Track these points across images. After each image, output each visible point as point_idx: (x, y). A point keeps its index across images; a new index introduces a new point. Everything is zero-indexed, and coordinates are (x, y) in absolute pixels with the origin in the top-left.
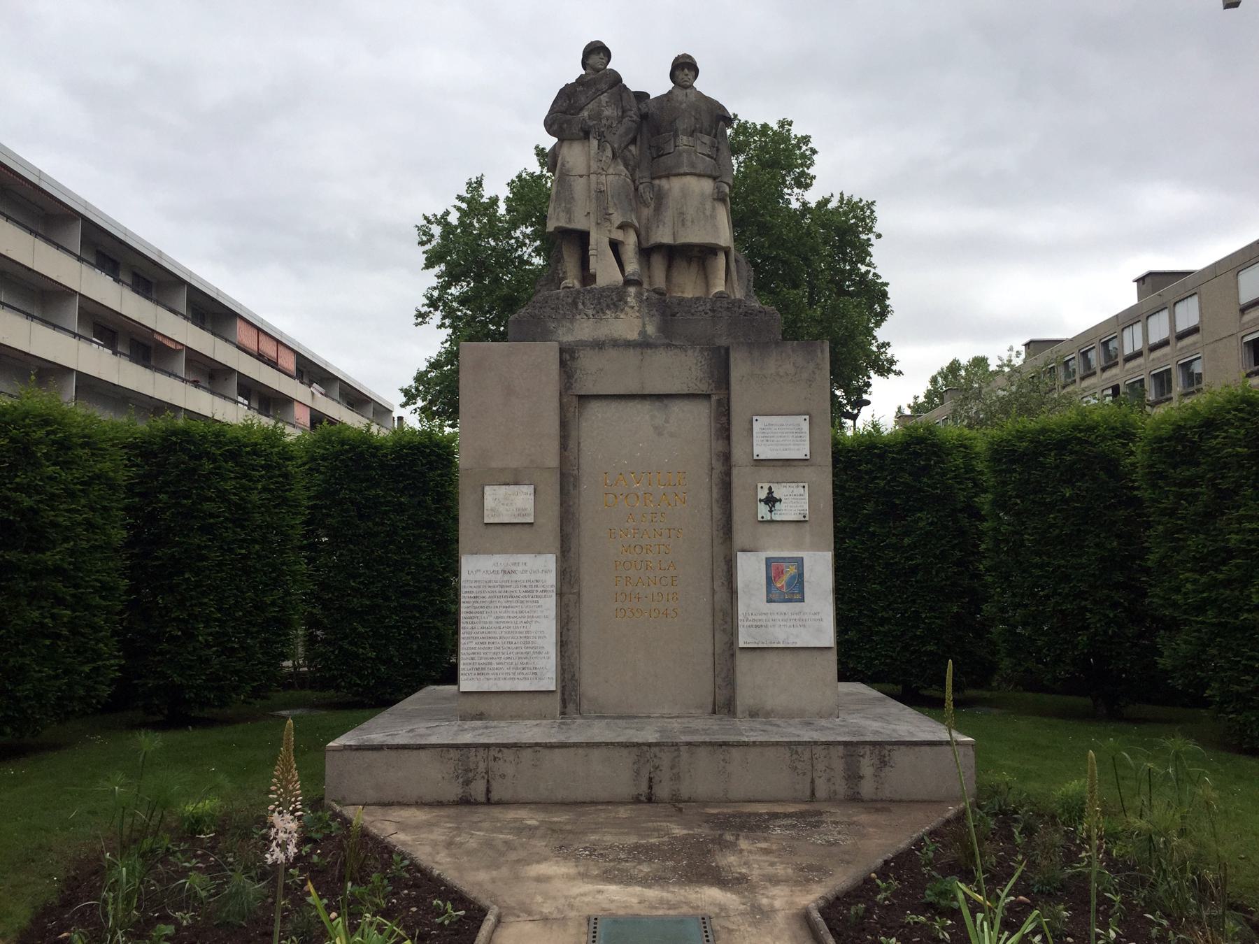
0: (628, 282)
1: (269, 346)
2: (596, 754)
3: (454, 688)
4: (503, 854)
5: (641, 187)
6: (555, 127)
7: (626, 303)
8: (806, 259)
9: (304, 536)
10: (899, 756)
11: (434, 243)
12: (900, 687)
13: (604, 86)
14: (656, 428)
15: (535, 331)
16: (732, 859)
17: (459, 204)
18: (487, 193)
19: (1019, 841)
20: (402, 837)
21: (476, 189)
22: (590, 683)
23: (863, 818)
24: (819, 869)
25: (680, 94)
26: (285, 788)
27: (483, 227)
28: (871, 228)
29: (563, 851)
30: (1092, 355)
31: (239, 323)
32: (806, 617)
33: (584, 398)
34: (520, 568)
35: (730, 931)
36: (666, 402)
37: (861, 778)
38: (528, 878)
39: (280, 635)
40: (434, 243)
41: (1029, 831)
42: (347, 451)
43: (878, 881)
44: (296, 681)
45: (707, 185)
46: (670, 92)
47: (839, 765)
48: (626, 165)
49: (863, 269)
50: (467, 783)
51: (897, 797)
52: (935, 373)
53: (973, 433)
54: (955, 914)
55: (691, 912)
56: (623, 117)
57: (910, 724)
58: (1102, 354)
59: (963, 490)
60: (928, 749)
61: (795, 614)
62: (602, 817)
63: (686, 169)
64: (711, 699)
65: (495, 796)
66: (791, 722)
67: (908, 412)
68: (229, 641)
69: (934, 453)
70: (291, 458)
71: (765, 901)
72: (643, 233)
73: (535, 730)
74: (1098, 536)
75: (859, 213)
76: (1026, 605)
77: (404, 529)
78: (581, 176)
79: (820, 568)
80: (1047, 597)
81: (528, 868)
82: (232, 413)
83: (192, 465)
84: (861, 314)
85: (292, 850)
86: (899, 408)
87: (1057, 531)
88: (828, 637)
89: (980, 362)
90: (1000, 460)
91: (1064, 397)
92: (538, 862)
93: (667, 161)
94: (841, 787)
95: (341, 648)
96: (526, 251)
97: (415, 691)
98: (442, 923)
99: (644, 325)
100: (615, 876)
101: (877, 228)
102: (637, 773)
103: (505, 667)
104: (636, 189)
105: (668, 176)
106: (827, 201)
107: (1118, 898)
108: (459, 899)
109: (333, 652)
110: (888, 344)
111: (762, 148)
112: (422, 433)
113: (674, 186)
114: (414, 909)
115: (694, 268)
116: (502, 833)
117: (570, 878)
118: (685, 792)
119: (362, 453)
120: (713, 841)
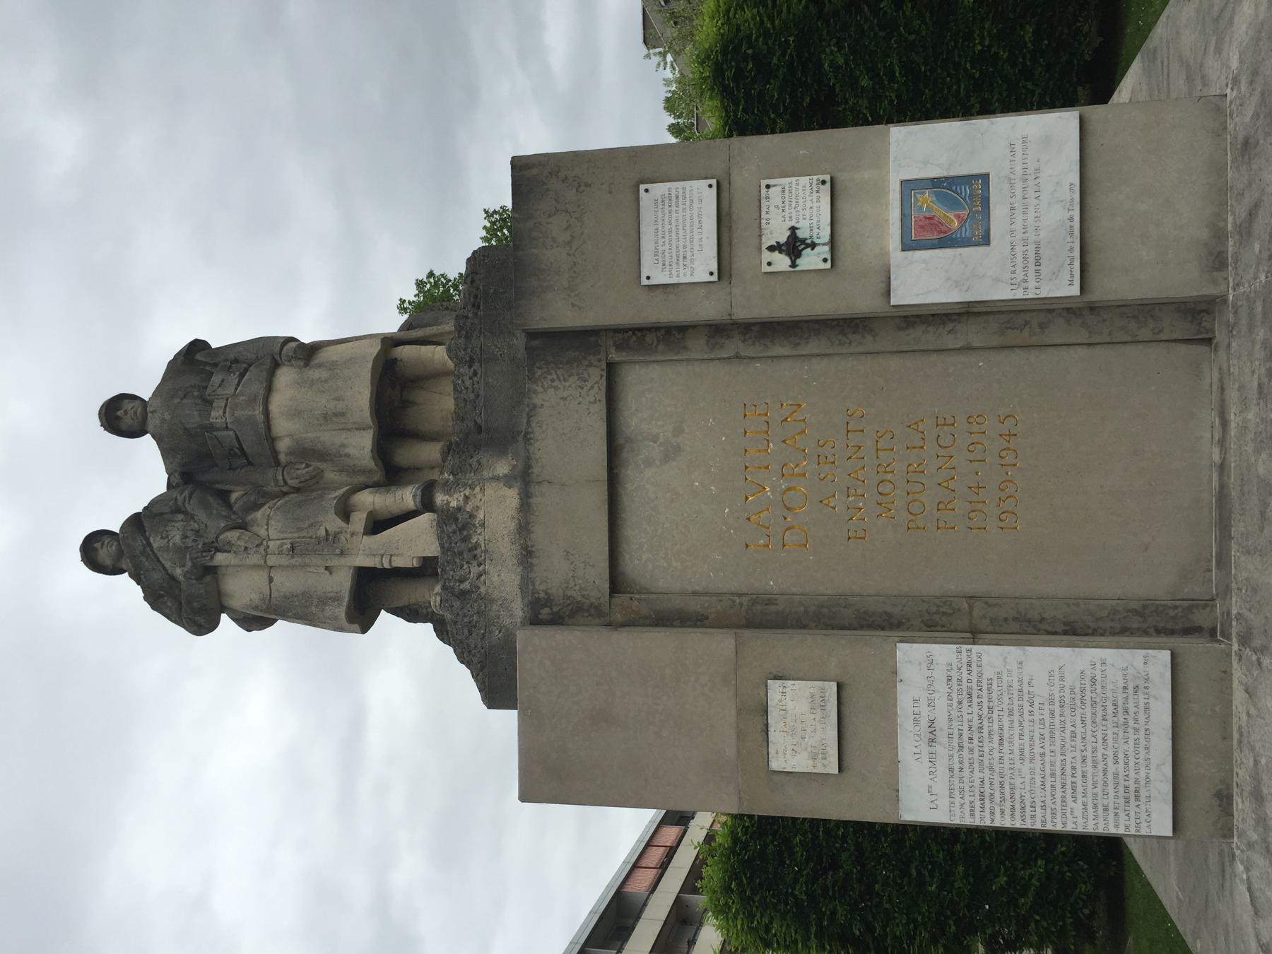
7: (459, 509)
13: (139, 542)
14: (666, 458)
22: (1153, 580)
25: (152, 422)
32: (1019, 170)
33: (617, 583)
34: (925, 711)
36: (621, 441)
42: (740, 884)
46: (154, 437)
48: (256, 507)
56: (185, 513)
63: (258, 412)
64: (1183, 349)
72: (362, 479)
78: (271, 580)
79: (921, 149)
88: (1061, 125)
99: (496, 478)
105: (271, 440)
109: (1037, 922)
113: (283, 427)
115: (419, 396)
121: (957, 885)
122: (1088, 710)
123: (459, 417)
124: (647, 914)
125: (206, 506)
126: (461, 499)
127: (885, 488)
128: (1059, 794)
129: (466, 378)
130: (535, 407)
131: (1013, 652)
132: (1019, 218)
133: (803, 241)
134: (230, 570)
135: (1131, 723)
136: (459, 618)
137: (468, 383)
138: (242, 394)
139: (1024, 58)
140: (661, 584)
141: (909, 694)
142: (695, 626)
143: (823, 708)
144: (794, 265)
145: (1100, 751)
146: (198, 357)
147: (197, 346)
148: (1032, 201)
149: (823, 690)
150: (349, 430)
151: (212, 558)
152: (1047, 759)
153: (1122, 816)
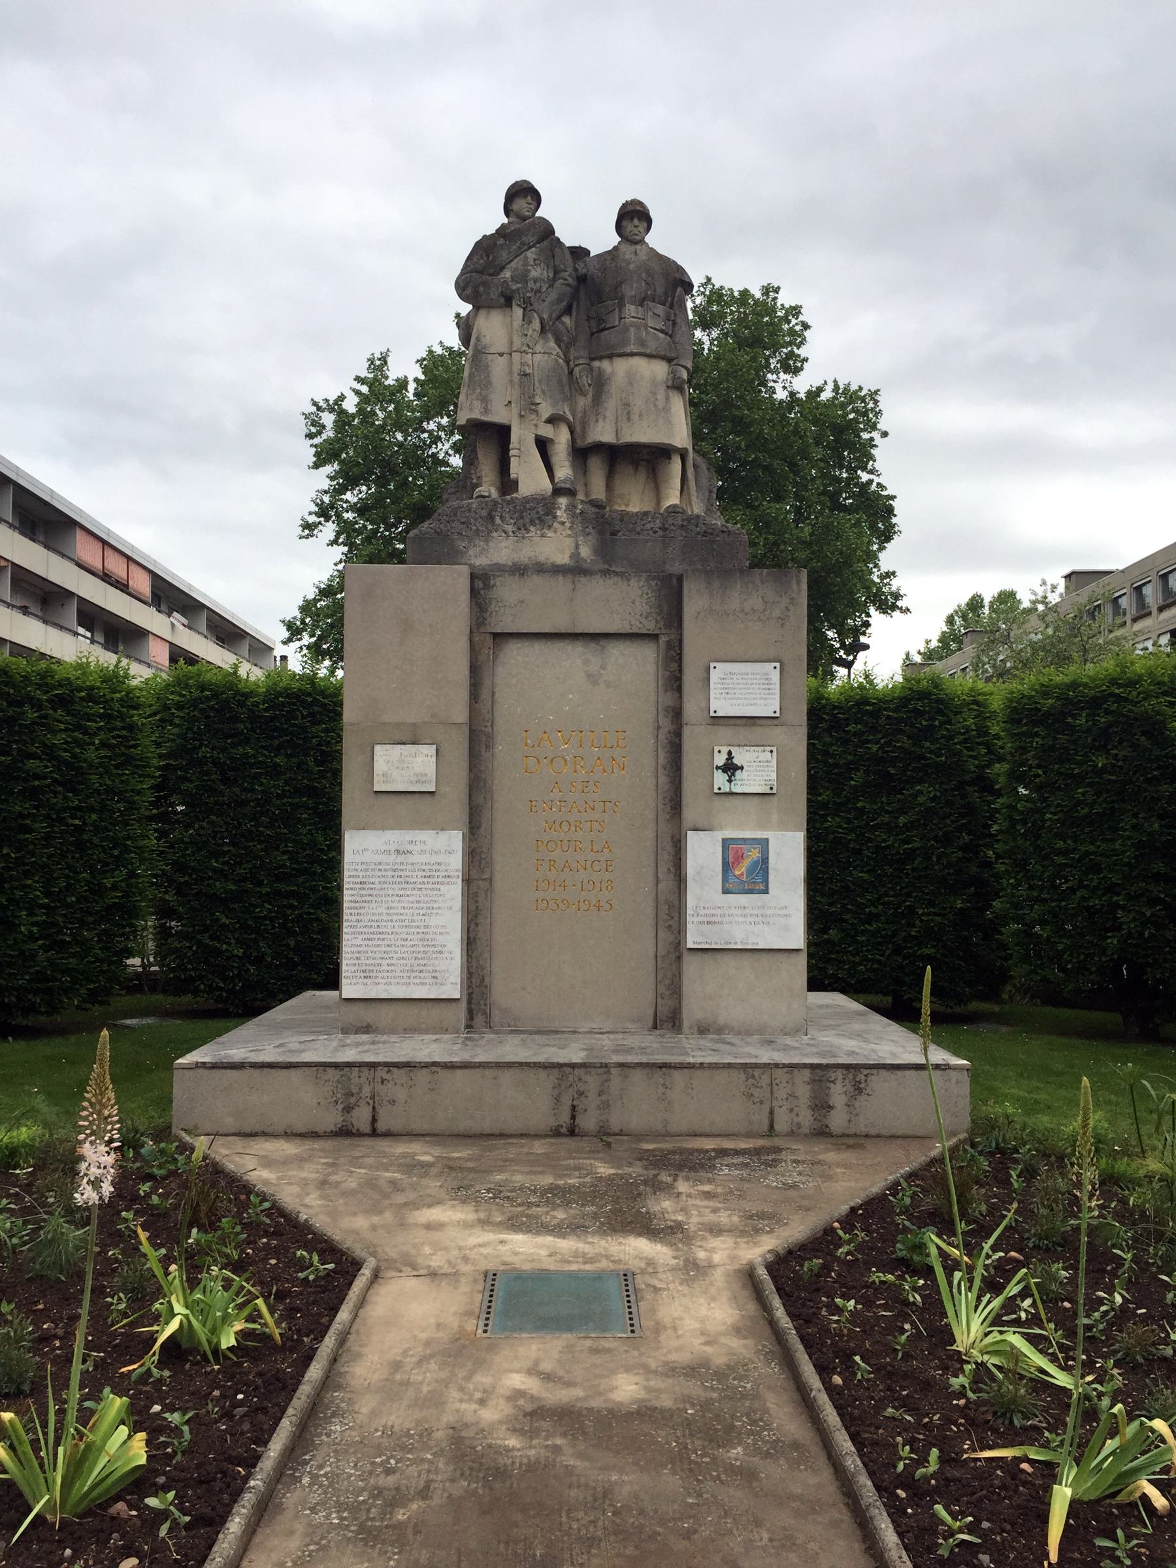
0: (558, 491)
1: (116, 563)
2: (507, 1076)
3: (336, 993)
4: (386, 1196)
5: (577, 370)
6: (469, 291)
7: (555, 517)
8: (793, 465)
9: (154, 804)
10: (879, 1083)
11: (324, 436)
12: (890, 999)
13: (531, 239)
14: (589, 676)
15: (438, 552)
16: (667, 1204)
17: (358, 386)
18: (393, 374)
19: (1016, 1185)
20: (265, 1174)
21: (380, 369)
23: (831, 1156)
24: (771, 1216)
25: (628, 249)
26: (99, 1113)
27: (388, 415)
28: (875, 424)
29: (461, 1193)
30: (1148, 591)
31: (79, 533)
32: (769, 912)
33: (500, 638)
34: (416, 848)
35: (656, 1290)
36: (602, 643)
37: (831, 1107)
38: (416, 1225)
39: (124, 927)
40: (324, 436)
41: (1029, 1173)
43: (840, 1232)
44: (141, 983)
45: (660, 369)
46: (615, 248)
47: (804, 1092)
48: (558, 341)
49: (864, 477)
50: (348, 1109)
51: (873, 1132)
52: (951, 611)
53: (990, 687)
54: (929, 1272)
55: (612, 1266)
56: (554, 279)
57: (895, 1044)
58: (1160, 588)
59: (974, 757)
60: (913, 1073)
61: (755, 906)
62: (512, 1152)
63: (632, 348)
64: (651, 1012)
65: (382, 1126)
66: (749, 1039)
67: (918, 659)
68: (60, 932)
69: (940, 712)
70: (137, 707)
71: (701, 1255)
72: (578, 429)
73: (434, 1046)
74: (1136, 816)
75: (859, 404)
76: (1045, 901)
77: (278, 796)
78: (501, 355)
79: (789, 853)
80: (1072, 890)
81: (417, 1213)
82: (67, 647)
83: (11, 713)
84: (860, 535)
85: (107, 1189)
86: (908, 654)
87: (1086, 810)
89: (1006, 598)
90: (1019, 721)
91: (1111, 643)
92: (430, 1206)
93: (610, 337)
94: (806, 1118)
95: (199, 943)
96: (443, 448)
97: (290, 996)
98: (307, 1278)
99: (577, 546)
100: (523, 1224)
101: (882, 425)
102: (557, 1099)
103: (398, 969)
104: (571, 373)
105: (610, 357)
106: (820, 390)
107: (1129, 1256)
108: (327, 1248)
109: (190, 948)
110: (894, 573)
111: (741, 321)
112: (303, 677)
113: (617, 369)
114: (273, 1262)
115: (642, 476)
116: (387, 1170)
117: (466, 1225)
118: (616, 1123)
119: (227, 701)
120: (645, 1182)
121: (218, 884)
122: (422, 949)
123: (624, 515)
124: (54, 558)
125: (560, 300)
127: (565, 827)
128: (366, 930)
129: (652, 525)
130: (629, 580)
131: (457, 903)
132: (739, 912)
133: (733, 774)
134: (508, 319)
135: (414, 974)
136: (473, 514)
137: (648, 526)
138: (648, 333)
139: (911, 948)
140: (500, 670)
141: (427, 837)
142: (471, 694)
143: (418, 782)
144: (718, 768)
145: (396, 956)
146: (679, 289)
148: (749, 919)
149: (429, 782)
152: (390, 924)
153: (353, 969)
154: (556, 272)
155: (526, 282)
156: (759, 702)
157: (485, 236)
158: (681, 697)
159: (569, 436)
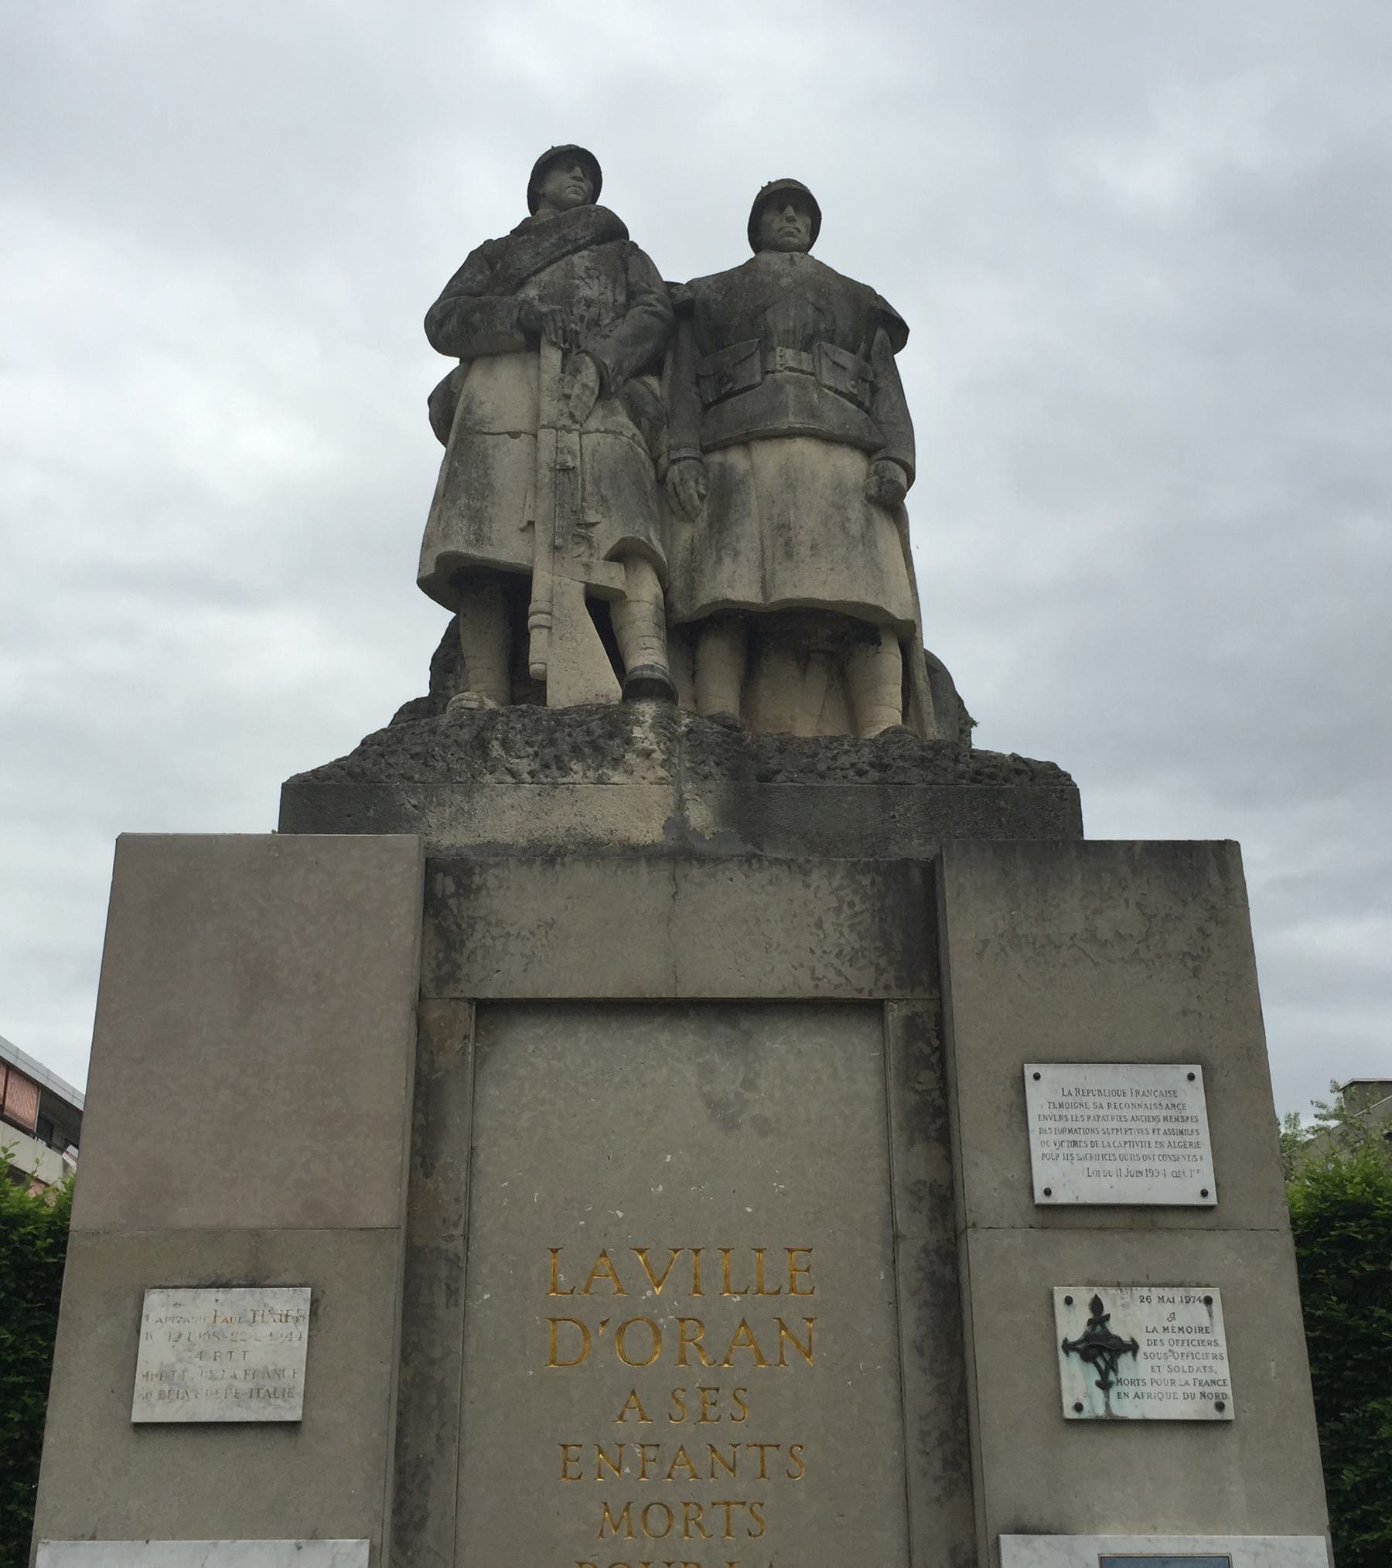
7: (629, 741)
13: (583, 235)
14: (713, 1104)
25: (775, 260)
36: (745, 1024)
48: (635, 414)
56: (627, 306)
63: (792, 421)
72: (679, 584)
78: (514, 435)
105: (745, 442)
113: (765, 463)
123: (785, 744)
125: (637, 338)
126: (646, 744)
129: (853, 758)
130: (806, 873)
133: (1112, 1366)
134: (532, 372)
137: (844, 760)
138: (821, 396)
142: (415, 1152)
143: (255, 1393)
144: (1068, 1347)
146: (880, 333)
147: (897, 332)
149: (288, 1393)
150: (762, 565)
151: (553, 344)
154: (631, 295)
155: (571, 306)
156: (1157, 1165)
157: (488, 242)
158: (949, 1158)
159: (658, 590)
